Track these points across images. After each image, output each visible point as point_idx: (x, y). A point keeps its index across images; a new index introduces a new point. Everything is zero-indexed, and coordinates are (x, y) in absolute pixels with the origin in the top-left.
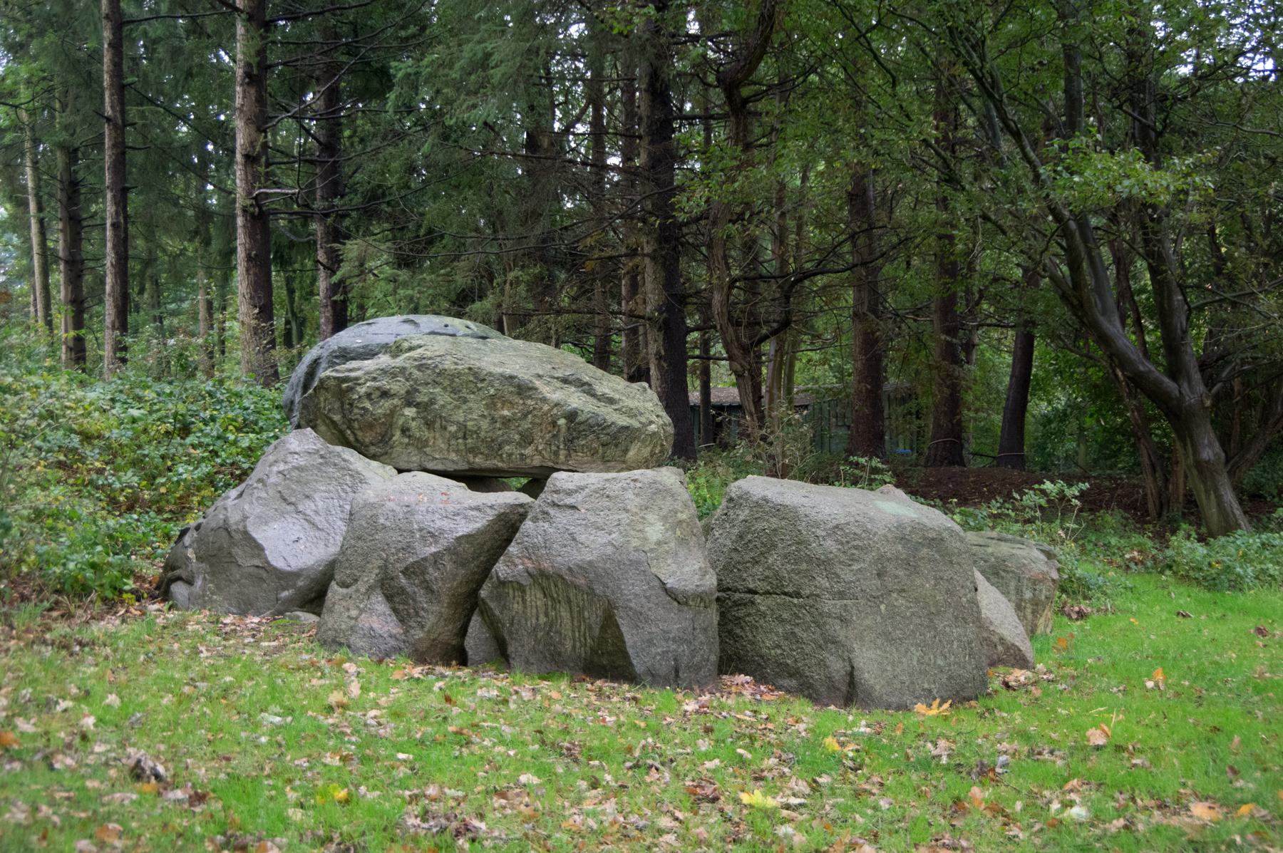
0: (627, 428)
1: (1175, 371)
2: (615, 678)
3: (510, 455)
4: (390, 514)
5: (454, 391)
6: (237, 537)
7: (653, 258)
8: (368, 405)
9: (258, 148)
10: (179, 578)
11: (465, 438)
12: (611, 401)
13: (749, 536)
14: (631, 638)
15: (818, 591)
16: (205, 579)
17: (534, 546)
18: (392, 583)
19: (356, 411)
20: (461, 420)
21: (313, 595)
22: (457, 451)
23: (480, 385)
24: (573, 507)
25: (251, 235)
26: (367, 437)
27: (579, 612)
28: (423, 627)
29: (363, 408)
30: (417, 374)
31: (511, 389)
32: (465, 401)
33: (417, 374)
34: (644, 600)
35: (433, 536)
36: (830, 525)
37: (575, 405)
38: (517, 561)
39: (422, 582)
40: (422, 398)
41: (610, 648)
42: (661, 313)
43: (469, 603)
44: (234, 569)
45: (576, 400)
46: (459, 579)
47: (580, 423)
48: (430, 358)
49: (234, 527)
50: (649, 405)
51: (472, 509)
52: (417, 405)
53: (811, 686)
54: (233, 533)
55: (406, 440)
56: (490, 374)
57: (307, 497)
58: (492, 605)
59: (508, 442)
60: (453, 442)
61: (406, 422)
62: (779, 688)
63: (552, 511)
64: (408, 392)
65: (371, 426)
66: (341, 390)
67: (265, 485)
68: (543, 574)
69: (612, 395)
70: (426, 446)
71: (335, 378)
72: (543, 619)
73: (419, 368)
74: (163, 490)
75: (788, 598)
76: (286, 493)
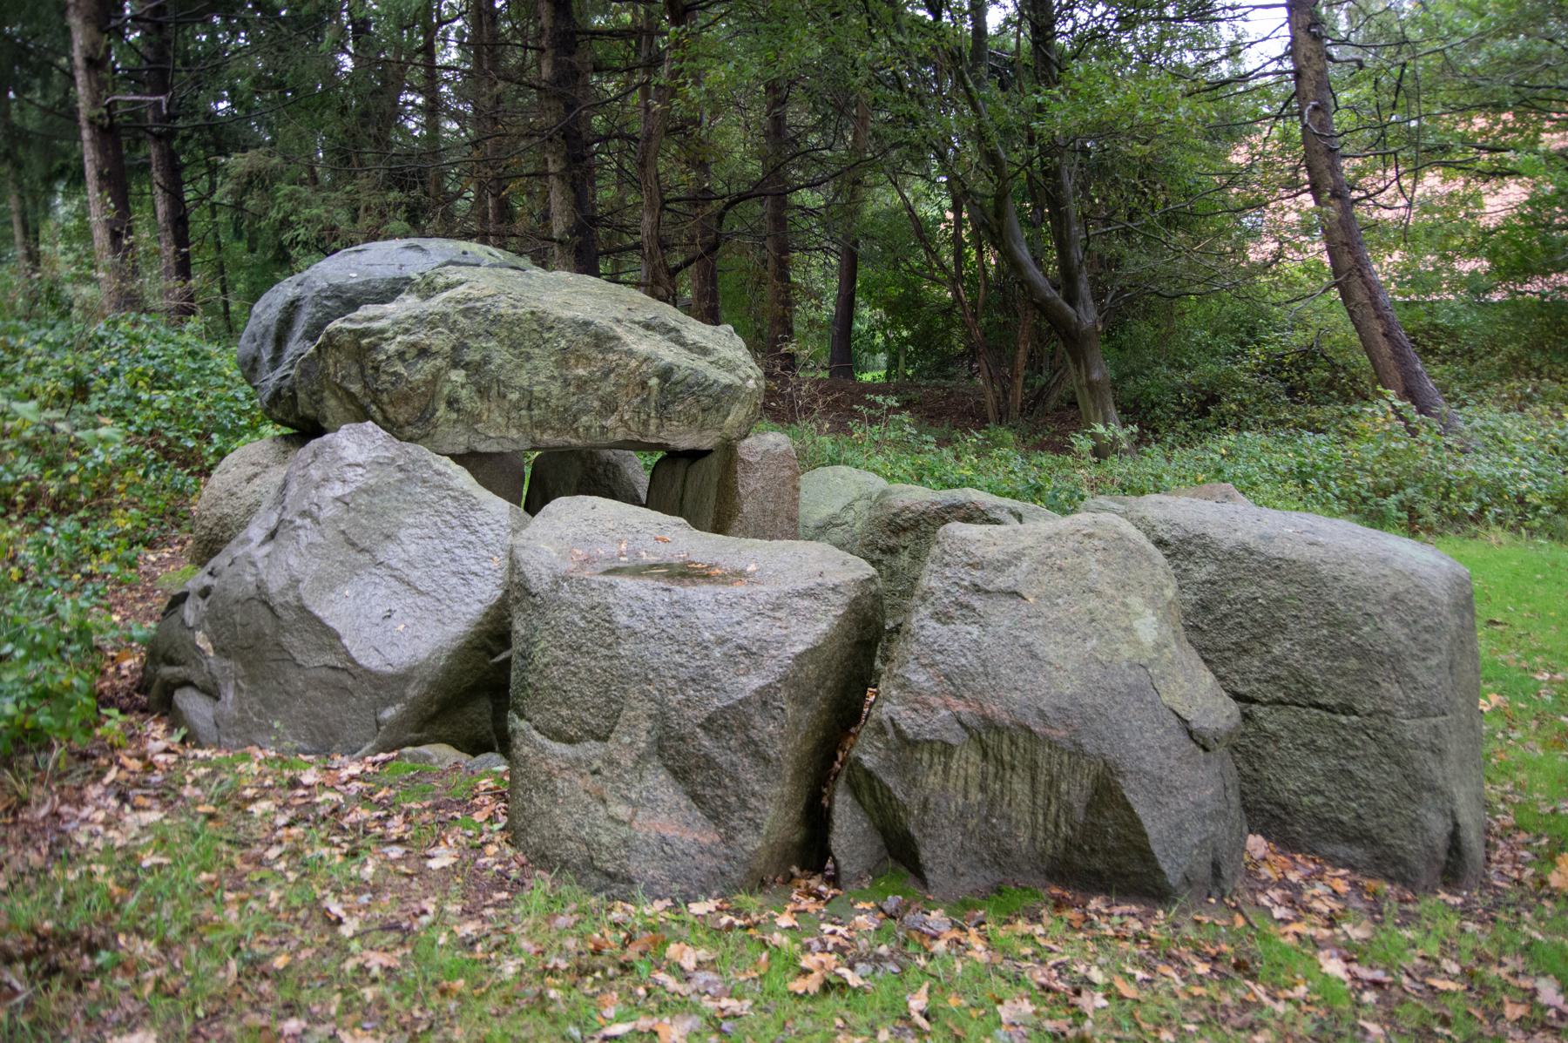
0: (729, 387)
1: (1072, 299)
3: (588, 429)
4: (636, 605)
5: (514, 345)
6: (289, 616)
7: (561, 177)
8: (400, 368)
9: (102, 52)
10: (186, 683)
11: (529, 408)
12: (704, 351)
13: (1224, 608)
14: (1154, 826)
15: (1388, 706)
16: (238, 688)
18: (683, 747)
19: (384, 377)
20: (526, 384)
21: (434, 708)
22: (519, 427)
23: (546, 335)
24: (1014, 594)
25: (101, 150)
26: (401, 414)
27: (1050, 784)
28: (757, 827)
29: (395, 374)
30: (463, 322)
31: (587, 339)
32: (529, 358)
33: (463, 322)
34: (1161, 755)
35: (749, 654)
36: (1385, 596)
37: (668, 360)
38: (935, 701)
39: (744, 745)
40: (472, 356)
41: (1111, 843)
42: (572, 236)
43: (825, 761)
44: (292, 673)
45: (668, 353)
46: (803, 727)
48: (478, 300)
49: (280, 600)
50: (740, 354)
51: (801, 595)
52: (466, 366)
53: (1401, 861)
54: (280, 611)
55: (454, 416)
56: (559, 320)
57: (388, 537)
58: (890, 781)
59: (586, 411)
60: (513, 414)
61: (453, 390)
62: (1334, 861)
64: (454, 348)
65: (406, 399)
66: (359, 346)
67: (316, 521)
68: (990, 724)
69: (704, 343)
70: (477, 422)
71: (350, 331)
72: (976, 796)
73: (465, 313)
74: (74, 480)
75: (1324, 714)
76: (354, 533)
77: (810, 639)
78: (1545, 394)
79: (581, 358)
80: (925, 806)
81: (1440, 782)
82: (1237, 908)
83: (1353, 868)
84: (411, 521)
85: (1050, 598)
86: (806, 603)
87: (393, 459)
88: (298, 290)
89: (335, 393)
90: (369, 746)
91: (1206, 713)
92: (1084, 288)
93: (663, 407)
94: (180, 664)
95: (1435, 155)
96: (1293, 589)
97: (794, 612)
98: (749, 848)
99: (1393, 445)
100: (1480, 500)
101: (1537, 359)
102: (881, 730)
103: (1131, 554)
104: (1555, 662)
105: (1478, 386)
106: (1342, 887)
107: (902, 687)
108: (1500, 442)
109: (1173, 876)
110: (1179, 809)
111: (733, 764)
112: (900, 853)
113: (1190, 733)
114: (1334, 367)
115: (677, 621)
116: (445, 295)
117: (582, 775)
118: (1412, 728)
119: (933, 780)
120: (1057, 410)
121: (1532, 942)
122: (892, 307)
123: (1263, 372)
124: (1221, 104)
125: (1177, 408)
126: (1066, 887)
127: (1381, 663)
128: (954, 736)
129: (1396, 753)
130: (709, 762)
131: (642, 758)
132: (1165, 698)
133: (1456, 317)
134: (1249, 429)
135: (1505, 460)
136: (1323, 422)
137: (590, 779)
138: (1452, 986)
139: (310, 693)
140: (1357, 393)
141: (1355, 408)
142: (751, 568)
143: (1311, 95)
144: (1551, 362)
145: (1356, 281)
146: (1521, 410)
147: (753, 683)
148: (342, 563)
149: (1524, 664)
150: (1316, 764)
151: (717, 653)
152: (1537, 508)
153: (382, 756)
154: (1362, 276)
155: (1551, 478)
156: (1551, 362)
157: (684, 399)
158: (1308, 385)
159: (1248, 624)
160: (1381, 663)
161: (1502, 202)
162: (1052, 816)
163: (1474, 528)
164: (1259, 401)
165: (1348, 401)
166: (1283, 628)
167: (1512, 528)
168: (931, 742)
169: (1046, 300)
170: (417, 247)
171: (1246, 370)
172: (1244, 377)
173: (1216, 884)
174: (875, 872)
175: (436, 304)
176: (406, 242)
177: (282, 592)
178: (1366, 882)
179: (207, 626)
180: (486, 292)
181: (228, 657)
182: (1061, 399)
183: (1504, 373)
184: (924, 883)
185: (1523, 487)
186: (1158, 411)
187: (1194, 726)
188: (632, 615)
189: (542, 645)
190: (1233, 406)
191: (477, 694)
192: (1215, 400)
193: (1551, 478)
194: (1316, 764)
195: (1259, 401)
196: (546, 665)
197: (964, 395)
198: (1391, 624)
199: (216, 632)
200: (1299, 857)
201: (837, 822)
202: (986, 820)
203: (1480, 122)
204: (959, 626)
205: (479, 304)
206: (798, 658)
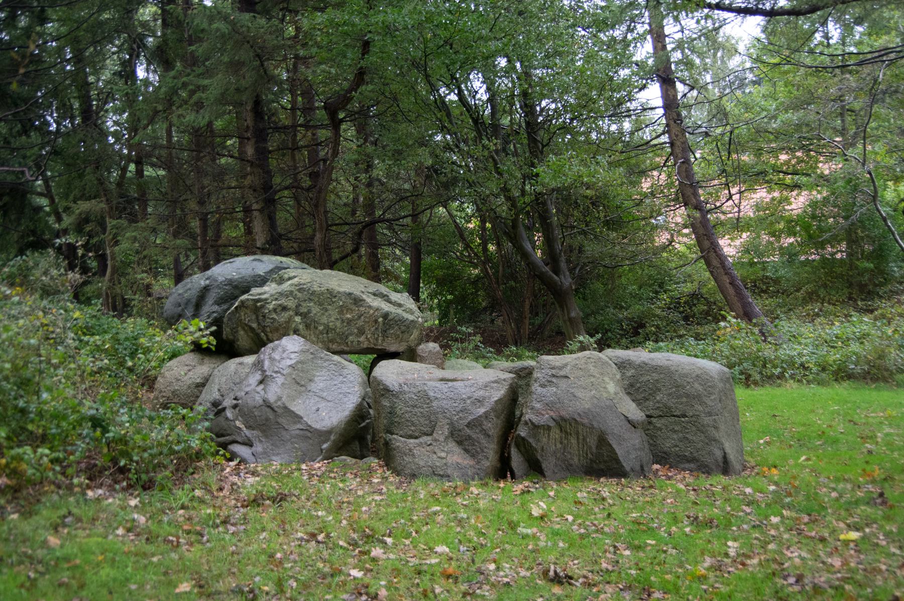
0: (412, 321)
1: (557, 271)
2: (612, 476)
3: (352, 342)
5: (321, 304)
6: (279, 411)
7: (261, 211)
8: (274, 316)
11: (327, 333)
12: (400, 305)
14: (620, 452)
17: (552, 402)
21: (341, 444)
24: (566, 377)
29: (272, 318)
30: (299, 295)
32: (327, 310)
35: (479, 401)
36: (693, 376)
40: (303, 310)
41: (606, 458)
44: (284, 433)
45: (386, 307)
52: (301, 315)
54: (276, 409)
56: (339, 292)
58: (531, 440)
59: (351, 334)
62: (684, 470)
63: (554, 380)
66: (256, 306)
68: (563, 419)
71: (252, 300)
72: (559, 446)
73: (300, 290)
76: (298, 379)
77: (499, 396)
83: (691, 471)
85: (578, 378)
88: (208, 282)
89: (243, 329)
92: (563, 265)
93: (384, 331)
95: (757, 176)
96: (662, 376)
97: (492, 388)
100: (782, 367)
102: (526, 423)
105: (790, 310)
107: (532, 409)
109: (628, 469)
110: (629, 447)
113: (629, 421)
116: (290, 282)
118: (707, 420)
119: (545, 440)
120: (550, 337)
122: (441, 282)
123: (669, 308)
124: (631, 156)
128: (552, 424)
129: (702, 430)
131: (447, 438)
134: (662, 341)
136: (705, 335)
143: (680, 155)
146: (813, 321)
147: (482, 411)
150: (675, 436)
154: (715, 252)
156: (830, 294)
161: (798, 203)
163: (779, 381)
164: (668, 325)
166: (660, 390)
167: (798, 381)
169: (542, 273)
170: (259, 260)
171: (660, 308)
172: (658, 312)
175: (286, 286)
177: (276, 402)
184: (544, 476)
186: (609, 334)
190: (653, 329)
191: (363, 438)
192: (642, 326)
194: (675, 436)
195: (668, 325)
197: (492, 331)
198: (696, 385)
203: (783, 157)
204: (549, 388)
206: (496, 402)
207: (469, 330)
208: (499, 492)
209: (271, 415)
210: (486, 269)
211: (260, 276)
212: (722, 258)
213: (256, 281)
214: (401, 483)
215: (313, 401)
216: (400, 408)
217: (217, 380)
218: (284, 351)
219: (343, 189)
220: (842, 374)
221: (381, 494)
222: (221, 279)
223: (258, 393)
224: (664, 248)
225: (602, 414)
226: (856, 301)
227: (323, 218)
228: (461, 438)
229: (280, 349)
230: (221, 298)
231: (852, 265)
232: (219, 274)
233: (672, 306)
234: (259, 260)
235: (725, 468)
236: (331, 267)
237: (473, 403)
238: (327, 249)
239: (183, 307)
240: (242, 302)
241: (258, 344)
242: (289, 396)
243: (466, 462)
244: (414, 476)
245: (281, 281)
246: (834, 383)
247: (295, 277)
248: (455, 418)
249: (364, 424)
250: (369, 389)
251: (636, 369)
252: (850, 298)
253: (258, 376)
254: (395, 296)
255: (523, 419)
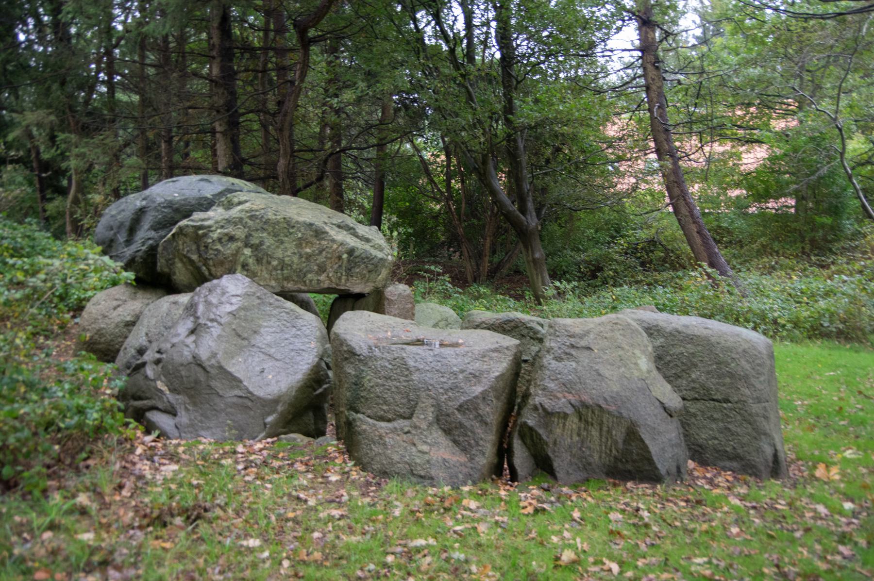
0: (381, 259)
1: (523, 210)
2: (642, 480)
3: (311, 281)
4: (417, 357)
5: (276, 235)
6: (213, 372)
7: (224, 133)
8: (219, 247)
11: (282, 270)
12: (367, 240)
13: (669, 358)
14: (654, 449)
15: (744, 398)
16: (187, 409)
17: (570, 381)
18: (448, 419)
19: (211, 252)
21: (290, 417)
22: (276, 280)
23: (291, 231)
28: (484, 454)
29: (217, 250)
30: (250, 223)
32: (282, 242)
35: (475, 376)
36: (740, 350)
39: (476, 417)
40: (254, 241)
41: (635, 457)
42: (232, 170)
44: (217, 400)
47: (356, 257)
48: (257, 211)
52: (251, 246)
53: (754, 467)
54: (209, 369)
56: (297, 222)
57: (255, 332)
58: (541, 431)
59: (310, 272)
60: (274, 273)
62: (724, 469)
64: (246, 237)
66: (197, 235)
67: (220, 324)
69: (367, 236)
71: (193, 226)
72: (576, 438)
73: (251, 218)
75: (716, 403)
76: (239, 331)
77: (500, 369)
78: (781, 265)
79: (309, 243)
80: (555, 443)
81: (768, 431)
82: (689, 485)
83: (733, 472)
84: (265, 324)
85: (602, 350)
86: (496, 354)
87: (255, 293)
89: (181, 260)
90: (263, 434)
91: (670, 400)
92: (530, 205)
93: (349, 270)
94: (147, 398)
96: (699, 348)
97: (491, 359)
98: (481, 463)
99: (706, 293)
100: (754, 322)
101: (776, 246)
102: (535, 408)
103: (634, 331)
104: (803, 397)
105: (746, 261)
106: (730, 479)
107: (544, 389)
108: (760, 291)
109: (663, 471)
110: (663, 443)
111: (472, 426)
112: (544, 466)
113: (665, 409)
114: (666, 250)
115: (439, 364)
116: (240, 207)
117: (398, 435)
118: (755, 408)
119: (558, 431)
120: (508, 276)
121: (811, 494)
122: (401, 214)
123: (626, 253)
125: (578, 274)
126: (615, 479)
127: (740, 380)
128: (569, 410)
129: (749, 419)
130: (461, 425)
131: (430, 425)
132: (654, 394)
133: (732, 222)
135: (765, 300)
136: (662, 282)
137: (405, 436)
138: (784, 508)
139: (229, 410)
140: (680, 265)
141: (680, 273)
142: (461, 341)
143: (655, 100)
144: (784, 248)
145: (682, 202)
147: (478, 390)
148: (235, 345)
149: (789, 398)
150: (714, 426)
151: (461, 376)
152: (784, 326)
153: (269, 440)
154: (685, 200)
155: (790, 310)
156: (784, 248)
157: (359, 266)
158: (652, 262)
159: (680, 365)
160: (740, 380)
161: (753, 158)
162: (608, 447)
164: (626, 270)
165: (675, 269)
166: (695, 366)
167: (771, 337)
168: (559, 413)
169: (509, 212)
171: (617, 252)
172: (616, 256)
173: (679, 476)
174: (533, 475)
175: (235, 212)
176: (199, 177)
177: (209, 359)
178: (740, 476)
179: (163, 378)
180: (261, 207)
181: (178, 394)
182: (510, 269)
183: (760, 253)
185: (776, 315)
187: (667, 405)
188: (416, 361)
189: (368, 377)
191: (317, 408)
192: (600, 269)
193: (790, 310)
194: (714, 426)
195: (626, 270)
196: (372, 387)
197: (451, 267)
198: (743, 363)
199: (169, 381)
200: (709, 468)
201: (516, 452)
202: (580, 449)
204: (566, 362)
205: (257, 213)
206: (497, 378)
207: (438, 270)
208: (500, 508)
209: (202, 377)
210: (449, 205)
211: (206, 199)
212: (691, 206)
213: (202, 205)
214: (368, 484)
215: (257, 359)
216: (369, 379)
217: (145, 322)
218: (224, 293)
219: (310, 117)
220: (816, 332)
221: (340, 505)
222: (159, 200)
223: (187, 346)
224: (627, 194)
225: (633, 399)
226: (809, 256)
227: (288, 143)
228: (450, 427)
229: (219, 291)
230: (159, 223)
231: (807, 219)
232: (158, 195)
233: (629, 251)
234: (207, 180)
235: (776, 468)
236: (295, 193)
237: (467, 379)
238: (291, 176)
239: (115, 230)
240: (181, 228)
241: (200, 278)
242: (226, 353)
243: (455, 459)
244: (385, 474)
245: (229, 205)
246: (808, 341)
247: (246, 201)
248: (443, 398)
249: (320, 391)
250: (328, 346)
251: (666, 338)
252: (803, 253)
253: (189, 324)
254: (362, 230)
255: (531, 402)
